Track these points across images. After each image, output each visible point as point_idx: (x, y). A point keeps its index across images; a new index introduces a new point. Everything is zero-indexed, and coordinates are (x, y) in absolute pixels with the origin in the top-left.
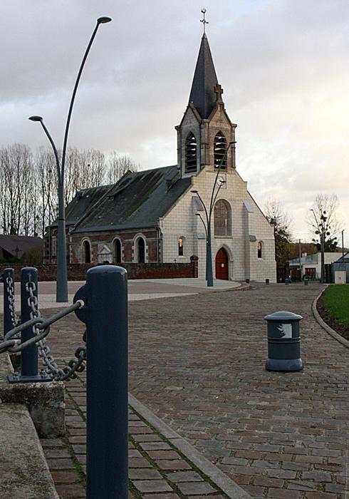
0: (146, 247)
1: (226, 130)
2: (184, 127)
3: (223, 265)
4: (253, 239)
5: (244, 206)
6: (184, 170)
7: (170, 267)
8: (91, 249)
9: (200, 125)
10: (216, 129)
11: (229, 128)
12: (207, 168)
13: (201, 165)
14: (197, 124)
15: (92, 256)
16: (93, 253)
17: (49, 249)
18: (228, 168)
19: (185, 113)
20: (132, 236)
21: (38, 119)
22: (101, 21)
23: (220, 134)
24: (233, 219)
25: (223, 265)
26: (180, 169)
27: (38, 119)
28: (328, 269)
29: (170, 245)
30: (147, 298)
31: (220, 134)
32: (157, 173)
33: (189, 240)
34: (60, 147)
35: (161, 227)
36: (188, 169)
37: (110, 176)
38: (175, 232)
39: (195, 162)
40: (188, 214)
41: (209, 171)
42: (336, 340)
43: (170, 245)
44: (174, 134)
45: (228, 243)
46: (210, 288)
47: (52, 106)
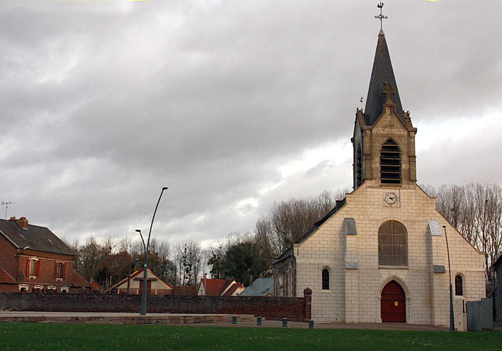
1: (400, 136)
3: (396, 304)
4: (440, 270)
5: (428, 228)
10: (384, 136)
11: (405, 133)
18: (404, 181)
19: (355, 122)
21: (139, 231)
22: (164, 189)
24: (409, 245)
25: (396, 304)
27: (139, 231)
29: (307, 277)
30: (118, 316)
33: (337, 270)
34: (146, 243)
35: (295, 255)
38: (317, 261)
40: (338, 239)
43: (307, 277)
45: (401, 275)
46: (259, 326)
47: (144, 226)
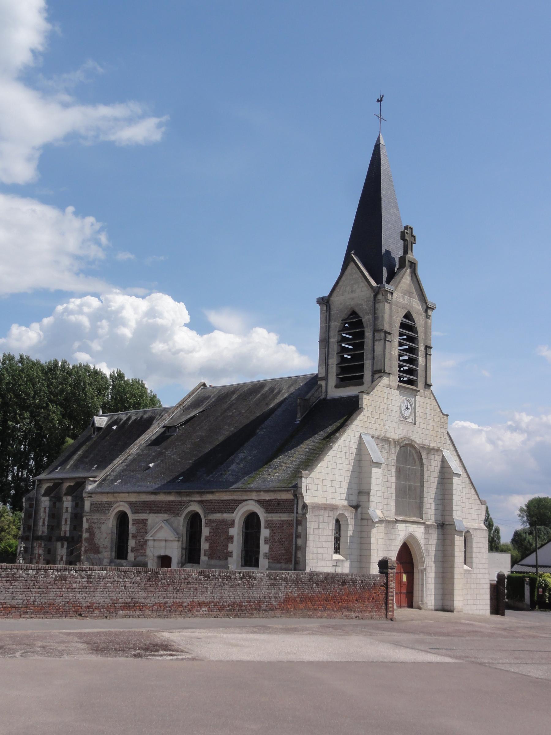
0: (265, 533)
2: (337, 300)
6: (332, 380)
7: (344, 583)
8: (132, 529)
9: (375, 296)
12: (385, 380)
13: (374, 372)
14: (369, 294)
15: (132, 543)
16: (134, 536)
17: (31, 522)
20: (231, 506)
23: (408, 316)
26: (326, 378)
28: (292, 511)
31: (408, 316)
32: (266, 389)
36: (342, 380)
37: (12, 424)
39: (361, 368)
41: (389, 387)
42: (108, 493)
44: (316, 311)
